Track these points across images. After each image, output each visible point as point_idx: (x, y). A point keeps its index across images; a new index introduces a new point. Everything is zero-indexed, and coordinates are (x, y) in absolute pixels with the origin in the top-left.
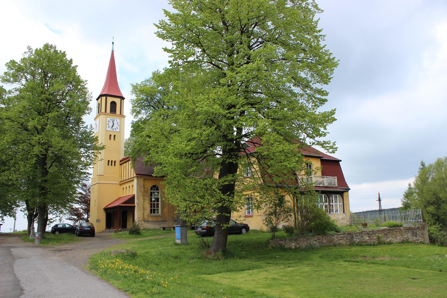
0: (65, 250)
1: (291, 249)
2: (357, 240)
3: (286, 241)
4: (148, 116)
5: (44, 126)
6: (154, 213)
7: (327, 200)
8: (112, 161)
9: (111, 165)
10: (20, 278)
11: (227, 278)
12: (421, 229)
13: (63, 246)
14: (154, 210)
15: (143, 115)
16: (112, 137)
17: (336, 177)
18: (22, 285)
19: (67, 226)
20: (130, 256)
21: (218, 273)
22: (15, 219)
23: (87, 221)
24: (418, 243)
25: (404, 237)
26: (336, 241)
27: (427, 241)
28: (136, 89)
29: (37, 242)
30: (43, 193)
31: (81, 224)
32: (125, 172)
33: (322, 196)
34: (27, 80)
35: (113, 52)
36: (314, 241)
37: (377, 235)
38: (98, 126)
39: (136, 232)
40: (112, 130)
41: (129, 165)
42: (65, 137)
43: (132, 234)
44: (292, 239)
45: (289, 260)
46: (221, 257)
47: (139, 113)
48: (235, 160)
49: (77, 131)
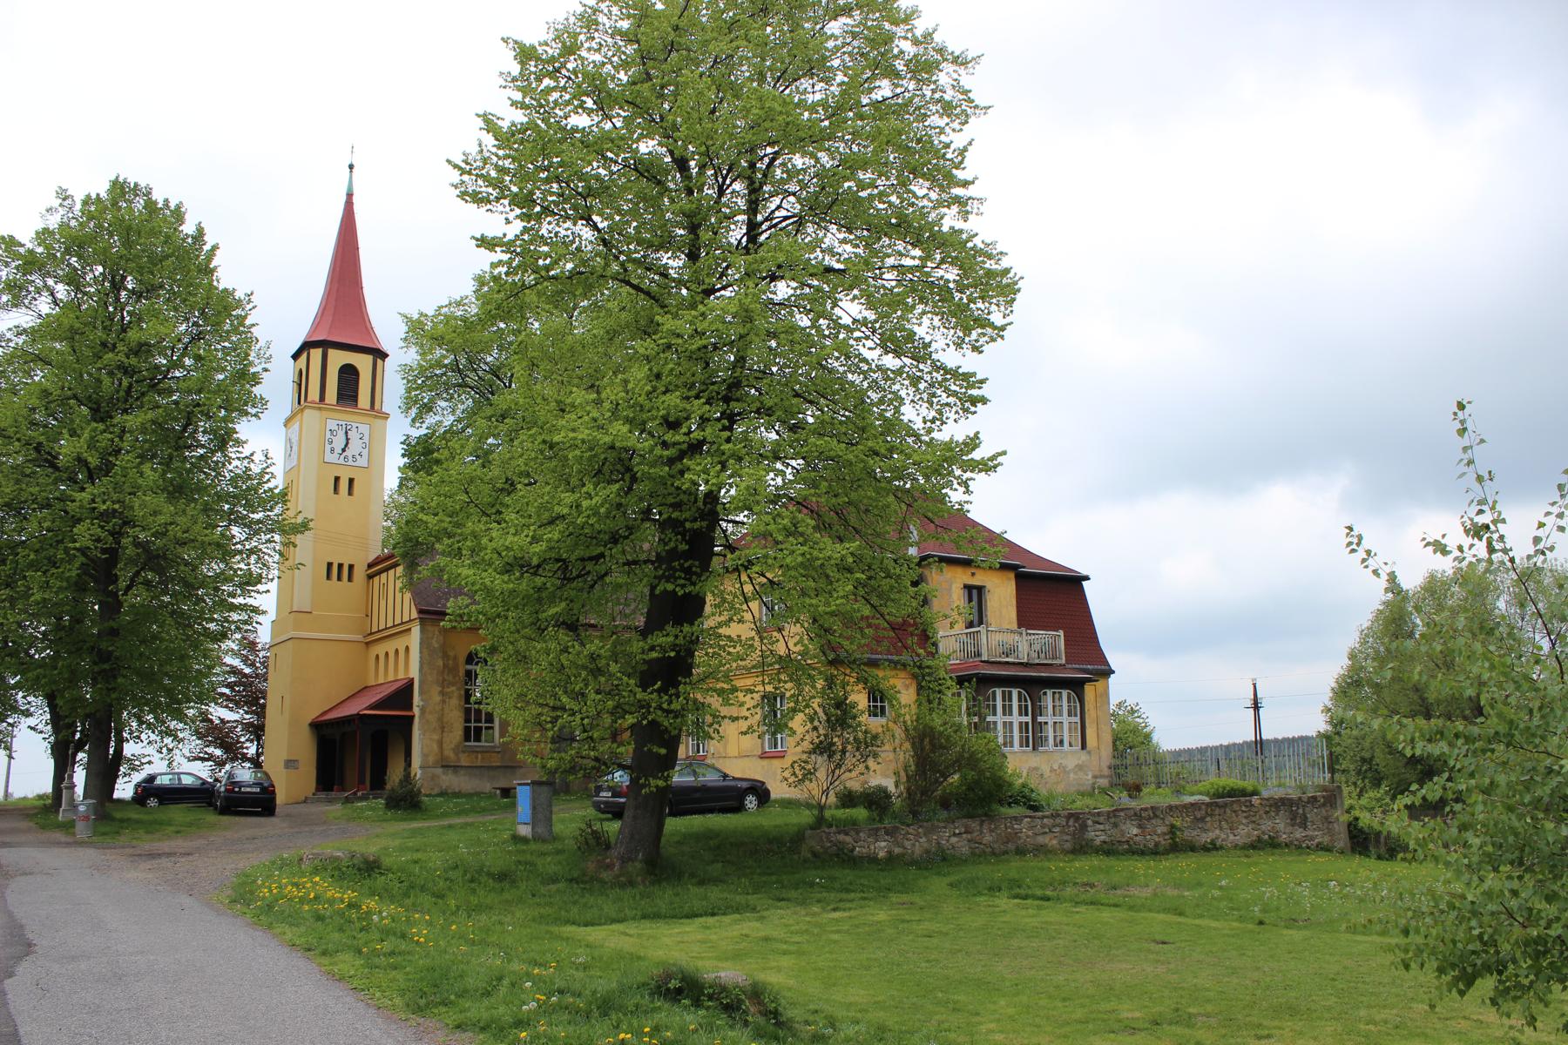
0: (169, 855)
1: (873, 860)
2: (1097, 835)
3: (857, 833)
4: (459, 420)
5: (110, 454)
6: (478, 739)
7: (1026, 706)
8: (340, 566)
9: (339, 579)
10: (24, 921)
11: (630, 936)
12: (1324, 805)
13: (167, 843)
14: (478, 730)
15: (444, 416)
16: (344, 485)
17: (1061, 633)
18: (30, 936)
19: (187, 781)
20: (359, 869)
21: (614, 921)
22: (10, 757)
23: (256, 763)
24: (1308, 847)
25: (1263, 827)
26: (1028, 837)
27: (1342, 840)
28: (417, 329)
29: (81, 830)
30: (104, 670)
31: (230, 775)
32: (383, 603)
33: (1010, 693)
34: (55, 302)
35: (350, 196)
36: (953, 837)
37: (1169, 820)
38: (295, 448)
39: (407, 802)
40: (341, 461)
41: (394, 579)
42: (179, 490)
43: (394, 807)
44: (878, 829)
45: (848, 891)
46: (639, 878)
47: (428, 408)
48: (683, 586)
49: (217, 467)
